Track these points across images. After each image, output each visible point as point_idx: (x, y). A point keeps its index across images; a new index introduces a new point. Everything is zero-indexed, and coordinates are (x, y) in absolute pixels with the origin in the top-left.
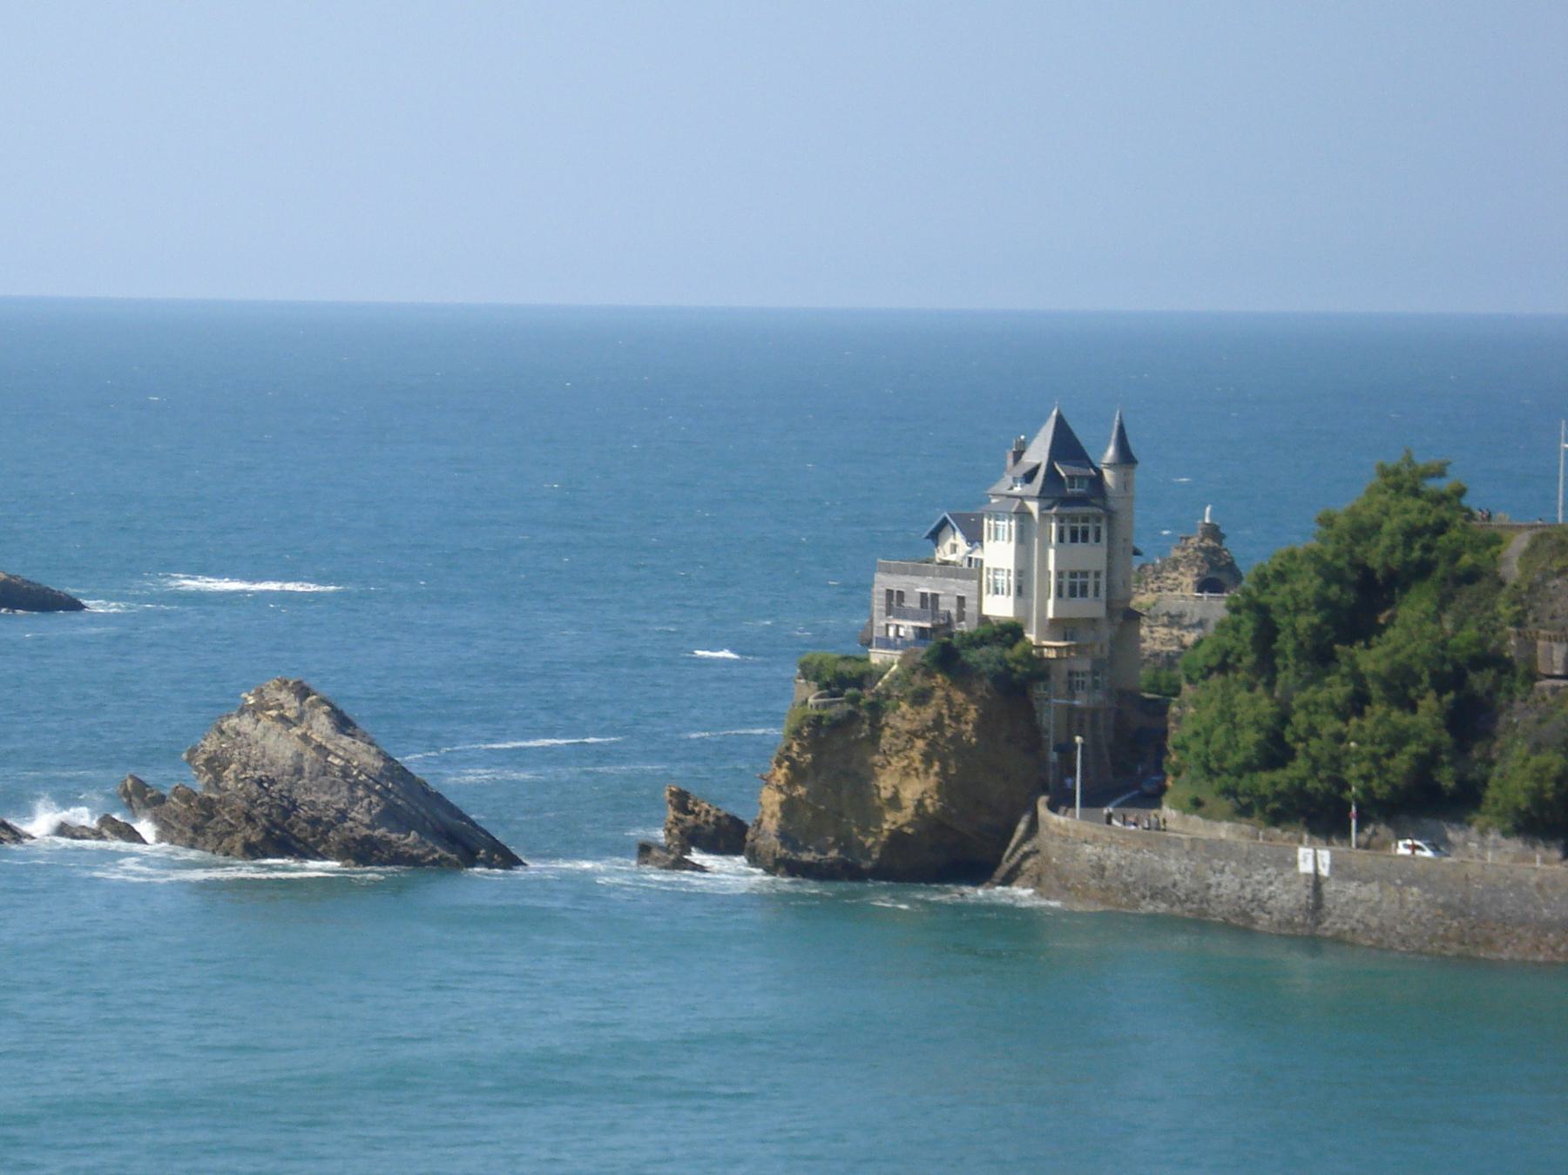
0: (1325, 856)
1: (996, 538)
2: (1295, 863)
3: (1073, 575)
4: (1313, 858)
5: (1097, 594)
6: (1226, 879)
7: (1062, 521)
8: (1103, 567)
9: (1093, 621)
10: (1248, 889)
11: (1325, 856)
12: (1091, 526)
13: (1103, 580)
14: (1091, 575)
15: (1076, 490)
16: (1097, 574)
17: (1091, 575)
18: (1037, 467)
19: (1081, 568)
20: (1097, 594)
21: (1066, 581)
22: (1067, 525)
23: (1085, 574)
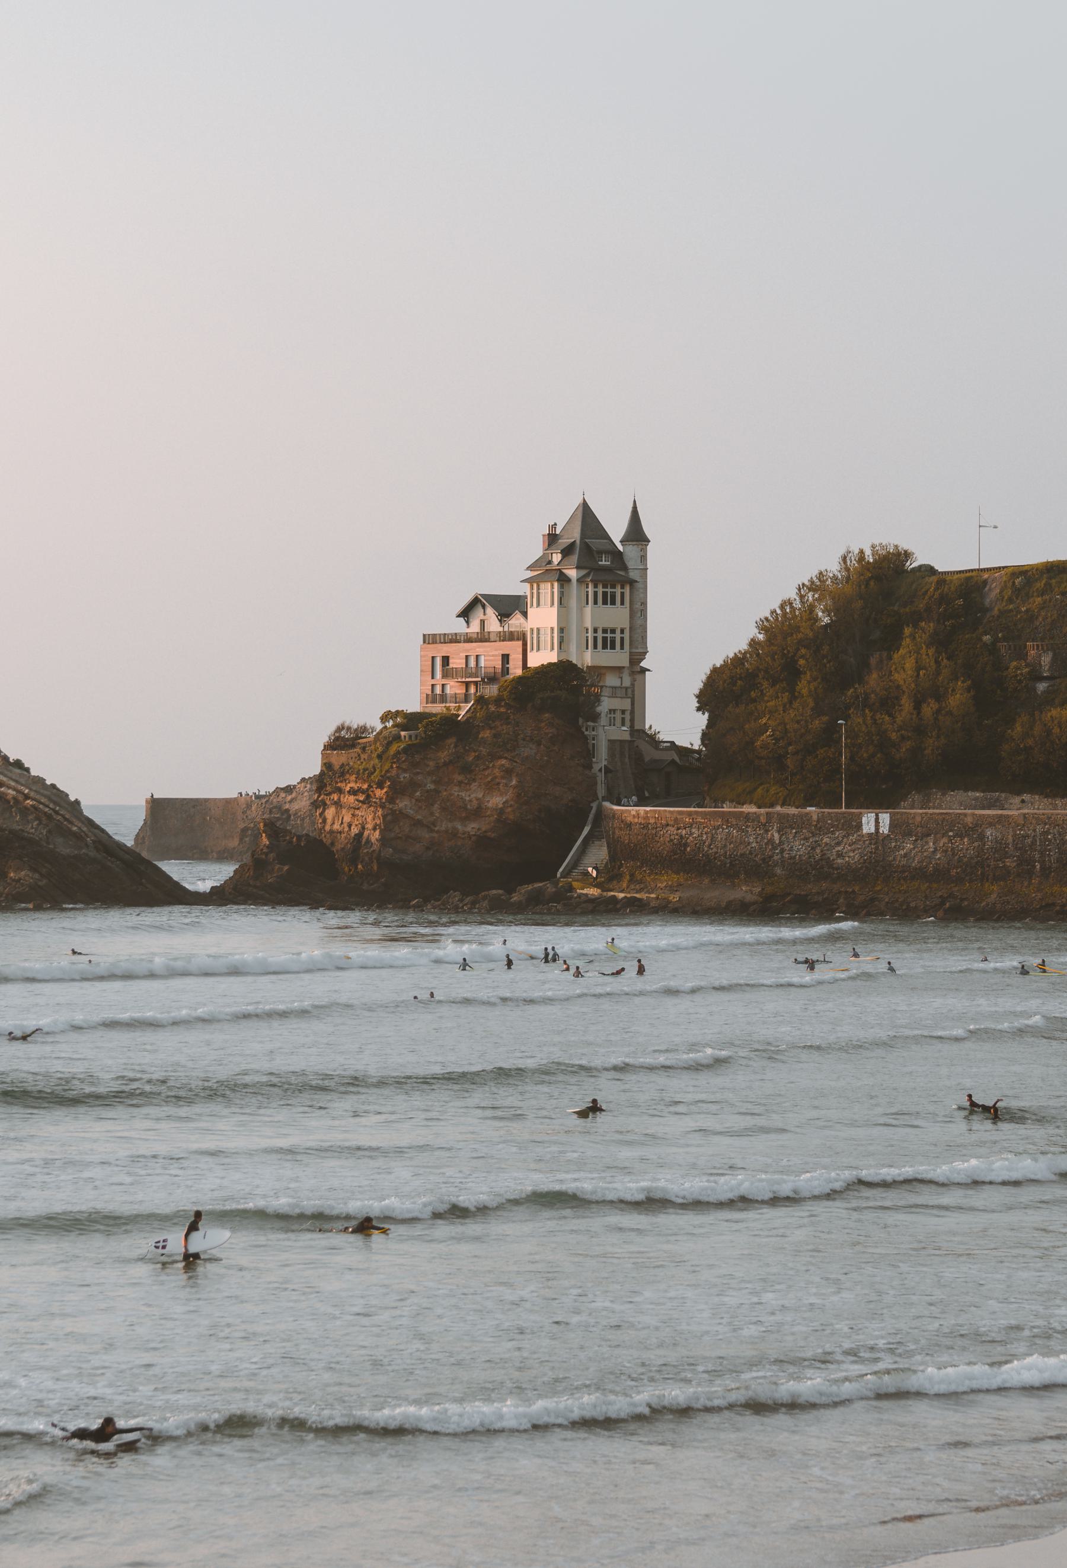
0: (885, 818)
1: (538, 605)
2: (859, 826)
3: (605, 631)
4: (874, 822)
5: (622, 648)
6: (252, 1404)
7: (596, 586)
8: (626, 625)
9: (619, 669)
10: (818, 851)
11: (885, 818)
12: (618, 591)
13: (627, 636)
14: (618, 631)
15: (603, 563)
16: (622, 631)
17: (618, 631)
18: (573, 544)
19: (612, 626)
20: (622, 648)
21: (600, 635)
22: (600, 590)
23: (613, 631)
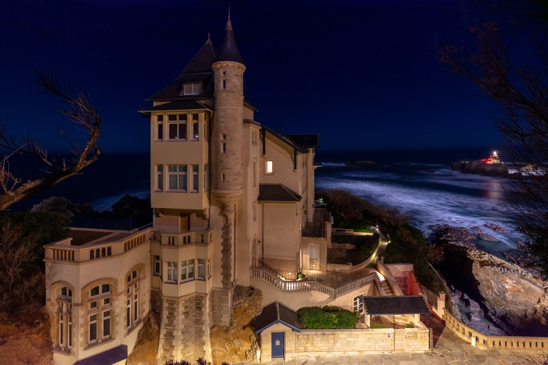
17: (190, 169)
